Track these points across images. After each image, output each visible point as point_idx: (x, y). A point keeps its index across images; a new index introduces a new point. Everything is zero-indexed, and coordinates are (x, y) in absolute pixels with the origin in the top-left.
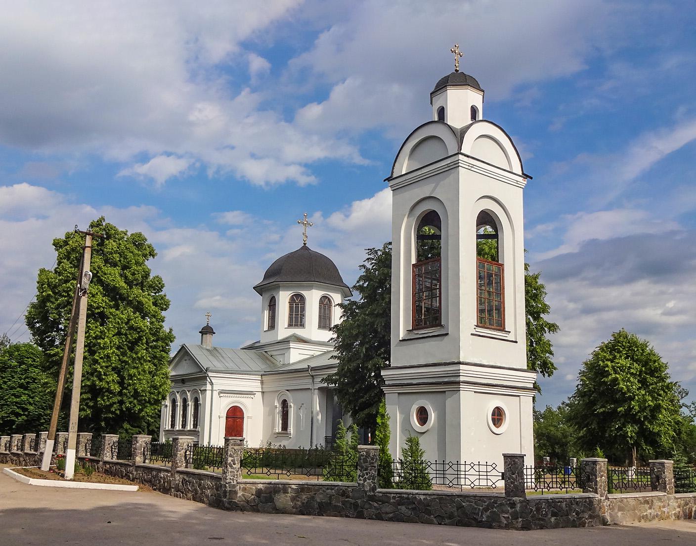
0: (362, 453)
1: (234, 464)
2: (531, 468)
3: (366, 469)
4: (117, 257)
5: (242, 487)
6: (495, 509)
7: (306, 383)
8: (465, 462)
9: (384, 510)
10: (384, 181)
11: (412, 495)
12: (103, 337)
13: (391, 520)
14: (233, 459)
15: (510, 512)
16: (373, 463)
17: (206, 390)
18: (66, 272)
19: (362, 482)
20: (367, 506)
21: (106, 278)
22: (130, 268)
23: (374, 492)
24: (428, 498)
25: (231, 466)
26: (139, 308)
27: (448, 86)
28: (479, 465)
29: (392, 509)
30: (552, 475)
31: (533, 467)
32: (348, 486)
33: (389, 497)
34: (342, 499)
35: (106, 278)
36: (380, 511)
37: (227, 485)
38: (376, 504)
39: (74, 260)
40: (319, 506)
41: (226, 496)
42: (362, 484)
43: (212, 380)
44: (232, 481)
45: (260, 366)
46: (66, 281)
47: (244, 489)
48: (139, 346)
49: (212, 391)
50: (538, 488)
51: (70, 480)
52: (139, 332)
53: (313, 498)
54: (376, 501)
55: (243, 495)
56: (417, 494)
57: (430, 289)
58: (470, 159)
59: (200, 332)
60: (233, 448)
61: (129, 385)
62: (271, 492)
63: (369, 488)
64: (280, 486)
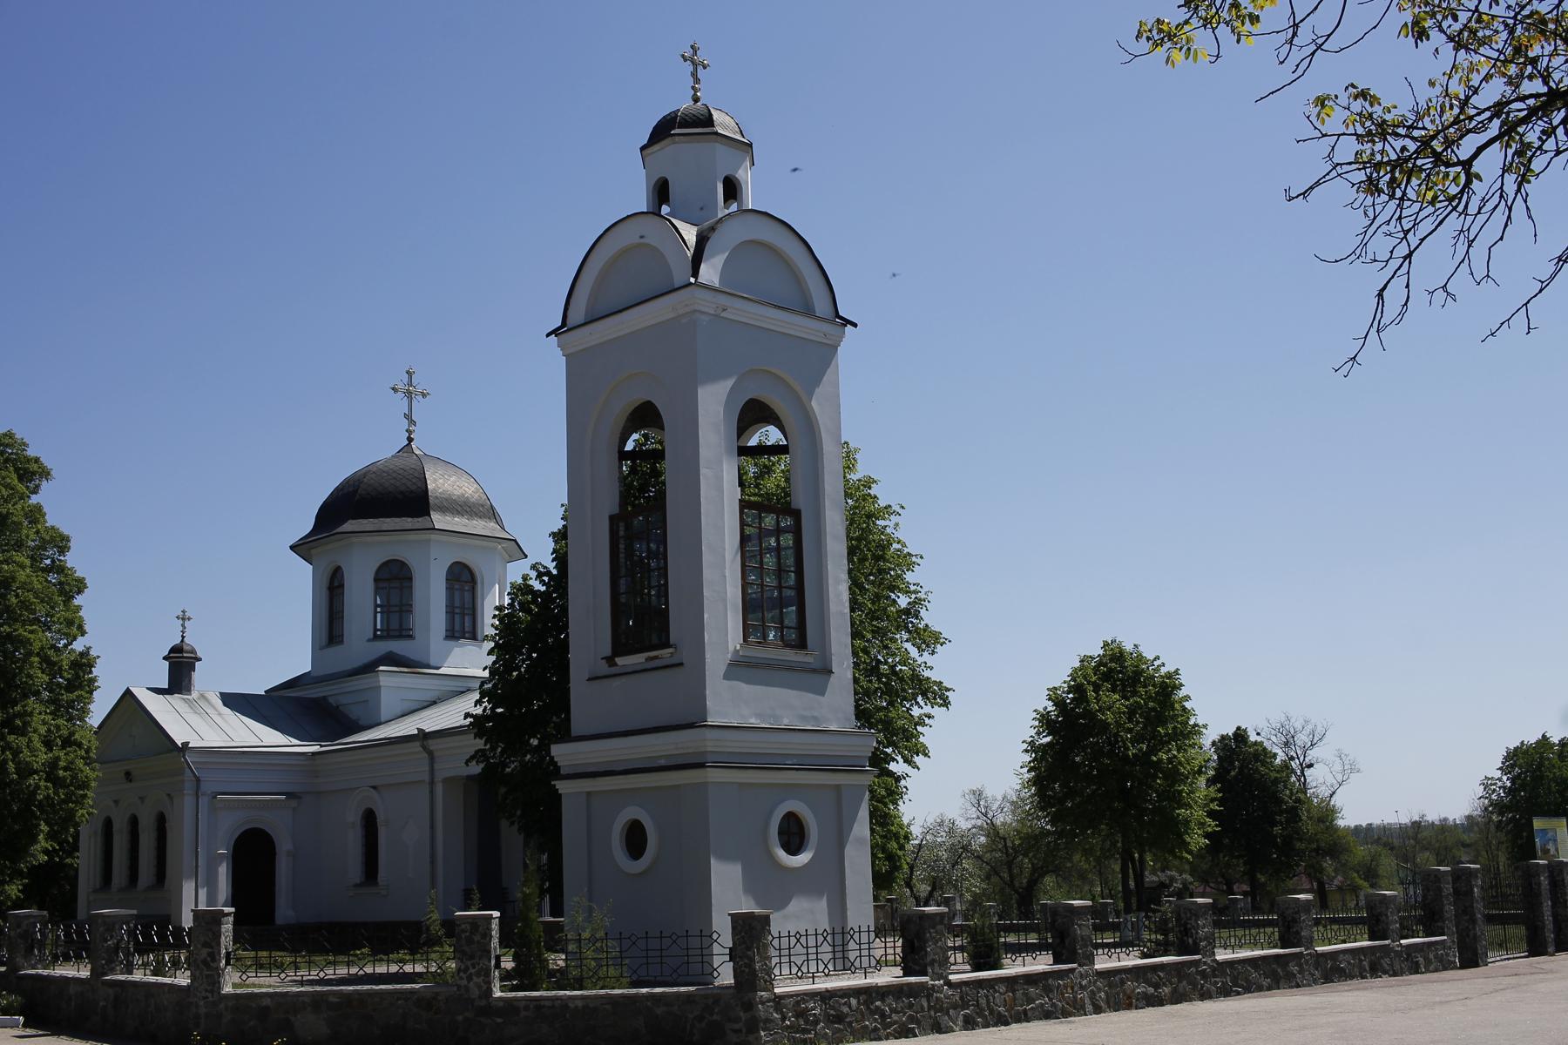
0: (463, 926)
3: (472, 957)
6: (715, 1017)
8: (701, 931)
10: (548, 335)
14: (210, 950)
19: (464, 982)
28: (661, 937)
31: (872, 928)
44: (209, 995)
50: (856, 969)
59: (164, 658)
64: (306, 1000)
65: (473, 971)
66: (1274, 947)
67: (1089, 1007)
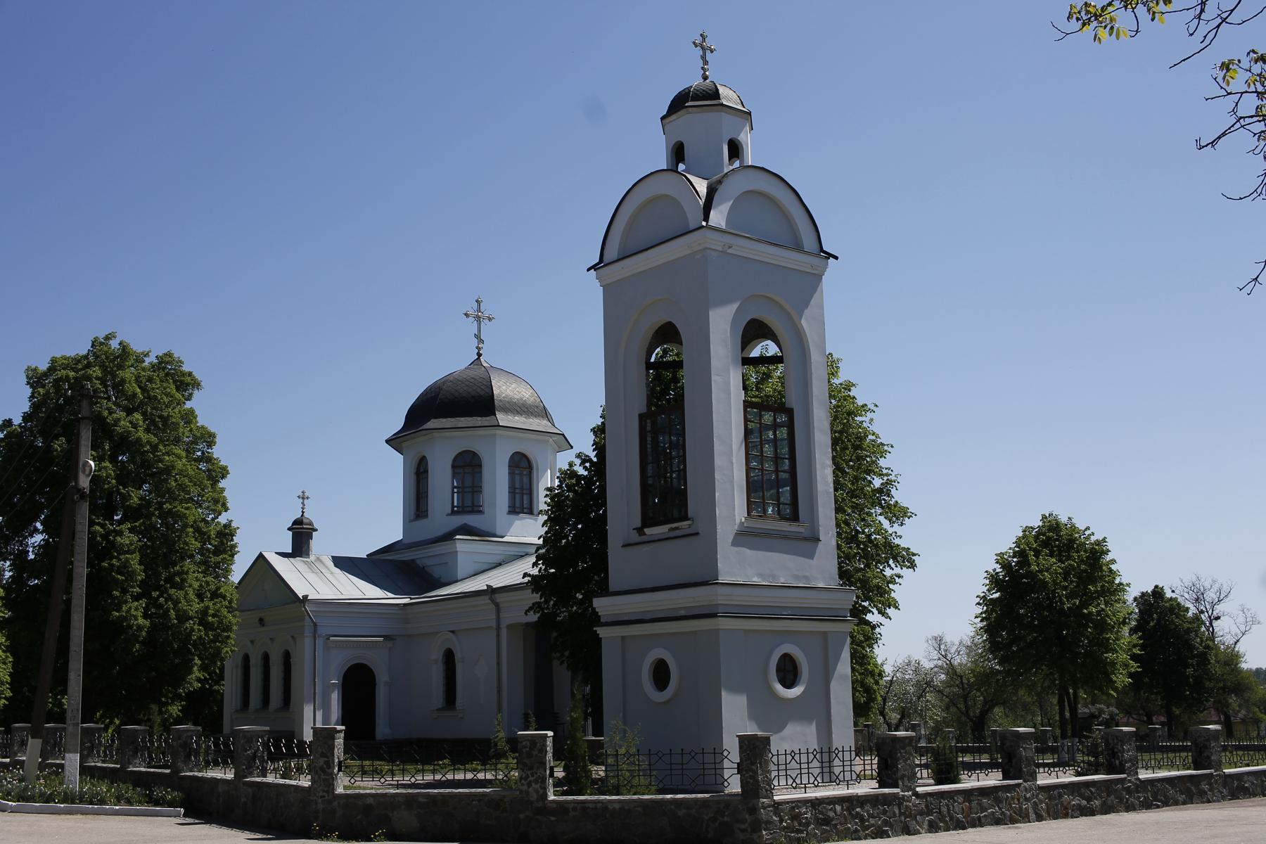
0: (524, 743)
2: (786, 754)
8: (682, 750)
10: (588, 270)
14: (326, 759)
15: (749, 821)
17: (304, 626)
19: (525, 788)
30: (864, 760)
31: (853, 749)
42: (526, 791)
44: (326, 795)
59: (289, 529)
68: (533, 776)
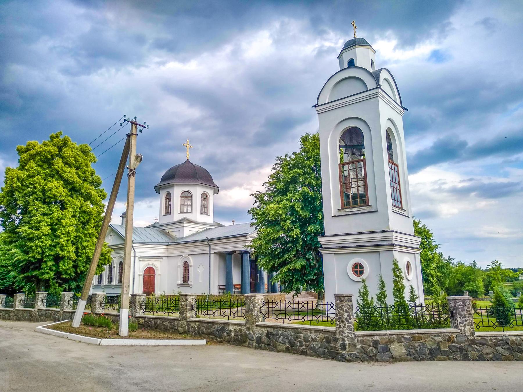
1: (350, 319)
3: (465, 317)
4: (72, 160)
5: (359, 339)
7: (205, 249)
9: (484, 351)
10: (313, 107)
11: (505, 337)
12: (64, 218)
13: (492, 359)
16: (469, 311)
18: (33, 170)
20: (470, 349)
21: (66, 175)
22: (82, 169)
23: (473, 336)
24: (519, 339)
25: (348, 321)
26: (88, 197)
27: (357, 45)
29: (491, 350)
32: (452, 333)
33: (486, 340)
34: (448, 344)
35: (66, 175)
36: (481, 353)
37: (346, 339)
38: (477, 347)
39: (39, 162)
40: (430, 352)
41: (346, 348)
42: (463, 330)
43: (135, 249)
45: (162, 239)
46: (32, 177)
47: (362, 342)
48: (88, 225)
49: (135, 256)
51: (125, 338)
52: (90, 215)
53: (424, 345)
54: (476, 344)
55: (362, 347)
56: (510, 336)
57: (169, 199)
58: (346, 99)
60: (348, 304)
61: (83, 253)
62: (387, 343)
63: (469, 333)
64: (395, 336)
65: (466, 323)
66: (232, 258)
67: (375, 360)
68: (466, 321)
